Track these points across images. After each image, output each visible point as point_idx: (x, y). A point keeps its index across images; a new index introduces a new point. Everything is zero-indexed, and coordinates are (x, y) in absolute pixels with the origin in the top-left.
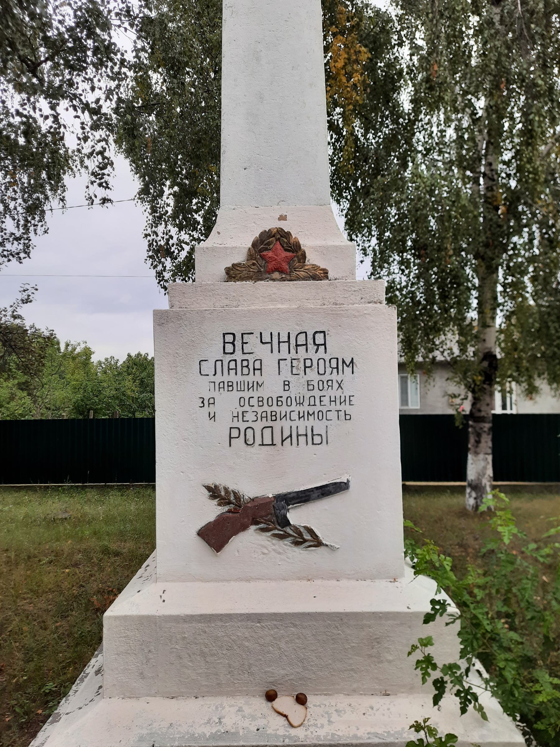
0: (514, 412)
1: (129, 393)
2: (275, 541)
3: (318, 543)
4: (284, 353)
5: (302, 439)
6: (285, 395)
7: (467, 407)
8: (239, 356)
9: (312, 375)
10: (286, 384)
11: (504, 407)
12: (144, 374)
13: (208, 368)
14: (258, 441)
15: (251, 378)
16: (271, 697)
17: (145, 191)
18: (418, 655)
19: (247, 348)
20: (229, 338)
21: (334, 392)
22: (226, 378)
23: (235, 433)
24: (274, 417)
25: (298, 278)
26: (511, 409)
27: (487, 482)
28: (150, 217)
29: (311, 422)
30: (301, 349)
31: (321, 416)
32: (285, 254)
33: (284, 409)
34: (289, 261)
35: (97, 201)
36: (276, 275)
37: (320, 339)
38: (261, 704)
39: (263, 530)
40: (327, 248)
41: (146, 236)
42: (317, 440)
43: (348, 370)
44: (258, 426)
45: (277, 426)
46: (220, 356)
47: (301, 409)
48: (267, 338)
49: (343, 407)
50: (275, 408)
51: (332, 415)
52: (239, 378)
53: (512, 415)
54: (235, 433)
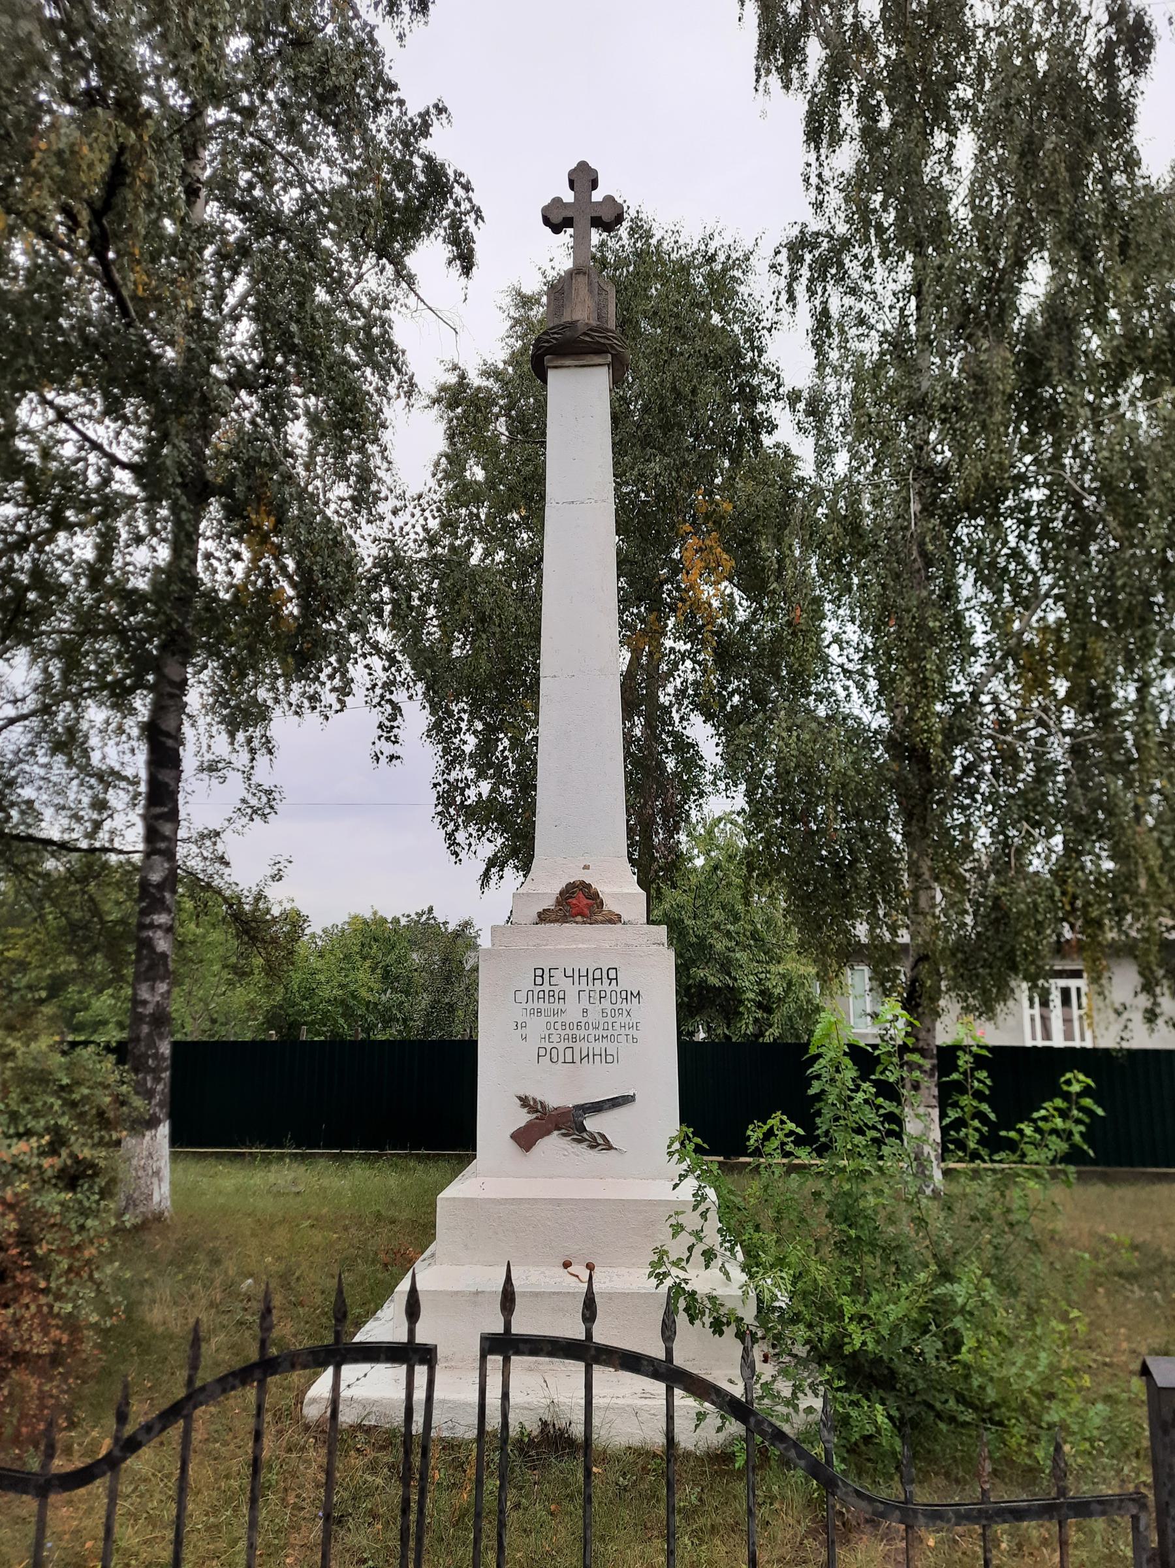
0: (1088, 1044)
1: (363, 993)
2: (574, 1144)
3: (610, 1147)
4: (583, 986)
5: (597, 1058)
6: (584, 1020)
7: (899, 1031)
8: (546, 987)
9: (606, 1004)
10: (585, 1011)
11: (1069, 1035)
12: (390, 959)
13: (521, 996)
14: (561, 1059)
15: (556, 1006)
16: (567, 1265)
17: (437, 726)
18: (673, 1221)
19: (553, 981)
20: (539, 972)
21: (624, 1019)
22: (536, 1005)
23: (542, 1052)
24: (574, 1038)
25: (596, 922)
26: (1083, 1039)
27: (930, 1152)
28: (442, 762)
29: (604, 1044)
30: (598, 982)
31: (611, 1038)
32: (586, 901)
33: (583, 1032)
34: (589, 906)
35: (383, 760)
36: (579, 918)
37: (612, 974)
38: (562, 1269)
39: (564, 1135)
40: (622, 895)
41: (435, 785)
42: (610, 1059)
43: (635, 1001)
44: (561, 1046)
45: (577, 1046)
46: (532, 987)
47: (597, 1032)
48: (569, 973)
49: (630, 1032)
50: (575, 1031)
51: (622, 1038)
52: (547, 1006)
53: (1083, 1049)
54: (542, 1052)
